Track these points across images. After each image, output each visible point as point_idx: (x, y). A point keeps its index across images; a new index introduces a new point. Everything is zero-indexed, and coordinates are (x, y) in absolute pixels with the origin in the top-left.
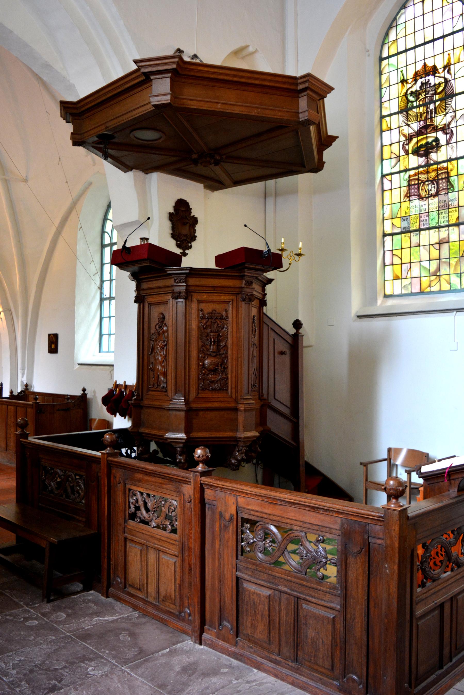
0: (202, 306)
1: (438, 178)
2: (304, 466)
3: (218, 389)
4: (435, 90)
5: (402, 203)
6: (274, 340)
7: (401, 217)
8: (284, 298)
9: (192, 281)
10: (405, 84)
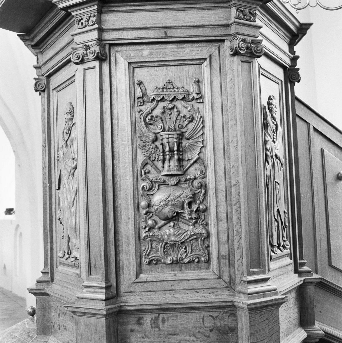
0: (141, 74)
3: (187, 260)
6: (322, 151)
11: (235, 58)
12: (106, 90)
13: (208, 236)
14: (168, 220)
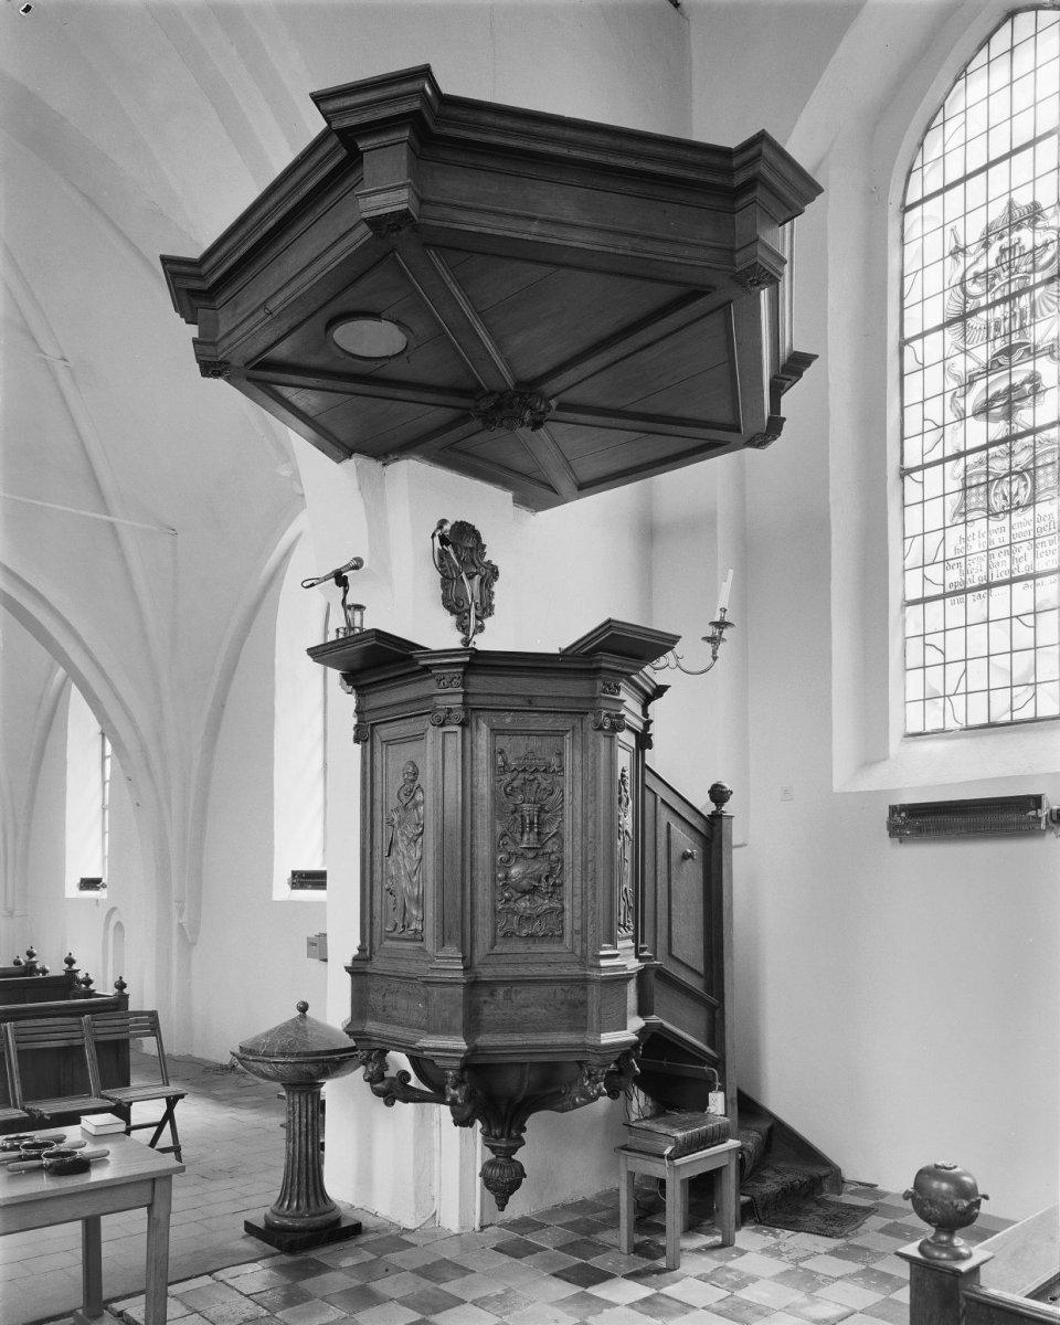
1: (1034, 464)
2: (735, 1101)
4: (1033, 261)
5: (947, 530)
7: (944, 561)
8: (691, 735)
9: (479, 683)
10: (961, 259)
11: (600, 733)
12: (467, 756)
13: (563, 910)
14: (525, 892)
